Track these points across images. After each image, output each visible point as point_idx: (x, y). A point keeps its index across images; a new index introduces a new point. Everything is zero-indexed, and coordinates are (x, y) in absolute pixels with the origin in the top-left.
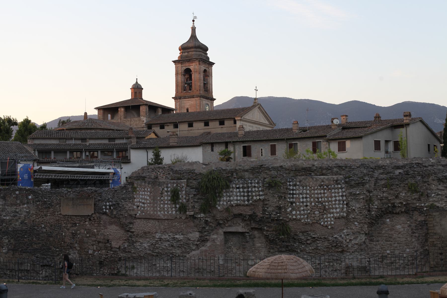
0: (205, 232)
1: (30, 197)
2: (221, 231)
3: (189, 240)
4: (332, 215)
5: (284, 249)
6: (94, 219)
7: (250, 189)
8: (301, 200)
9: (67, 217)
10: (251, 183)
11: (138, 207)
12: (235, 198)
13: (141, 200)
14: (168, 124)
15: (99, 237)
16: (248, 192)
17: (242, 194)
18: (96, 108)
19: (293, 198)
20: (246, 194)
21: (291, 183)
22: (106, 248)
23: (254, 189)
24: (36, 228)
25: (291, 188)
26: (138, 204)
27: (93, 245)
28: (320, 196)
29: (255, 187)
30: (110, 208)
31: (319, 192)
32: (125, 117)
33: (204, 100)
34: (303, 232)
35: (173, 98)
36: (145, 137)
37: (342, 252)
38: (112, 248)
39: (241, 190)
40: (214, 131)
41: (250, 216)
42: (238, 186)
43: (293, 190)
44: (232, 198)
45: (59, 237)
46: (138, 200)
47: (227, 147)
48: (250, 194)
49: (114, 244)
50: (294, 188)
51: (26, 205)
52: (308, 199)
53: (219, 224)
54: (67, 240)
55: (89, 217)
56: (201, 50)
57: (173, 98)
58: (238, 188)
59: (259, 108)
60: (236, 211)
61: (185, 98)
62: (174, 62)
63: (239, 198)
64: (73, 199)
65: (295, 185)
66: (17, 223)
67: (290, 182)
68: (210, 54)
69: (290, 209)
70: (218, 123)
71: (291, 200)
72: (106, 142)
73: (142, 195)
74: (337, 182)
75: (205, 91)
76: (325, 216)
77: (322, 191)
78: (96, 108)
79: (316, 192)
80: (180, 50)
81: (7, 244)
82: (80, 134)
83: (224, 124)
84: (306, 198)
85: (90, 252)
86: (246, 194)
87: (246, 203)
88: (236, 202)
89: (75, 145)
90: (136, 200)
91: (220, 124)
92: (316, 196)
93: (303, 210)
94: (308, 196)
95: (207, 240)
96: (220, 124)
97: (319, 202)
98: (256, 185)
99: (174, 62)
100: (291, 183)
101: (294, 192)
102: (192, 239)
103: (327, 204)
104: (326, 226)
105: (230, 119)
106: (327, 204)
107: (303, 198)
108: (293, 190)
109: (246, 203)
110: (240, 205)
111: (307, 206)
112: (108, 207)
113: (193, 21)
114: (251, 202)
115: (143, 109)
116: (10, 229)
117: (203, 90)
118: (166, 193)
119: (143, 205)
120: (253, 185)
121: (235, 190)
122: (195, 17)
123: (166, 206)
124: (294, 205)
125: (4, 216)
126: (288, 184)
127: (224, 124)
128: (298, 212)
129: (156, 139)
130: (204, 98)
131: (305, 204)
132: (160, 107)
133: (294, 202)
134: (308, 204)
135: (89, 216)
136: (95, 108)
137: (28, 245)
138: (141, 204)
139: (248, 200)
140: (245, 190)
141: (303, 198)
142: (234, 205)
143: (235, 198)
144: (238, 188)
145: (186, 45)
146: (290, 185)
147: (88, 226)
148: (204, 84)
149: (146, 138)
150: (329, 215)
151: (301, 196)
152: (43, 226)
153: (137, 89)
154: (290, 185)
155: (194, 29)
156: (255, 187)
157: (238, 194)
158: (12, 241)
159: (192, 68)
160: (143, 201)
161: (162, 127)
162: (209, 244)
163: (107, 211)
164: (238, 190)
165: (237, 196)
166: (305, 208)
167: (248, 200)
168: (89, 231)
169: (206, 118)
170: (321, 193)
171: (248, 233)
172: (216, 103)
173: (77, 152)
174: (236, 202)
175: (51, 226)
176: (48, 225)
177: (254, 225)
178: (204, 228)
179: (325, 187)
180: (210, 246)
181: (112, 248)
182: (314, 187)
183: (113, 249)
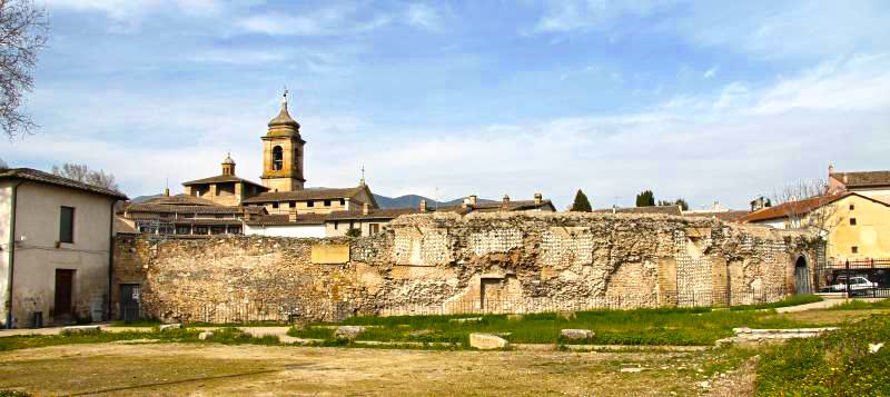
1: (275, 246)
18: (186, 185)
22: (362, 295)
32: (217, 194)
37: (586, 296)
40: (317, 212)
47: (352, 225)
54: (320, 289)
55: (344, 265)
60: (493, 258)
61: (274, 177)
70: (323, 203)
74: (585, 231)
78: (186, 185)
83: (329, 205)
85: (345, 300)
91: (326, 205)
96: (326, 205)
105: (336, 200)
115: (238, 187)
122: (287, 92)
127: (329, 205)
153: (230, 167)
159: (282, 145)
161: (276, 205)
162: (467, 289)
169: (327, 197)
172: (306, 186)
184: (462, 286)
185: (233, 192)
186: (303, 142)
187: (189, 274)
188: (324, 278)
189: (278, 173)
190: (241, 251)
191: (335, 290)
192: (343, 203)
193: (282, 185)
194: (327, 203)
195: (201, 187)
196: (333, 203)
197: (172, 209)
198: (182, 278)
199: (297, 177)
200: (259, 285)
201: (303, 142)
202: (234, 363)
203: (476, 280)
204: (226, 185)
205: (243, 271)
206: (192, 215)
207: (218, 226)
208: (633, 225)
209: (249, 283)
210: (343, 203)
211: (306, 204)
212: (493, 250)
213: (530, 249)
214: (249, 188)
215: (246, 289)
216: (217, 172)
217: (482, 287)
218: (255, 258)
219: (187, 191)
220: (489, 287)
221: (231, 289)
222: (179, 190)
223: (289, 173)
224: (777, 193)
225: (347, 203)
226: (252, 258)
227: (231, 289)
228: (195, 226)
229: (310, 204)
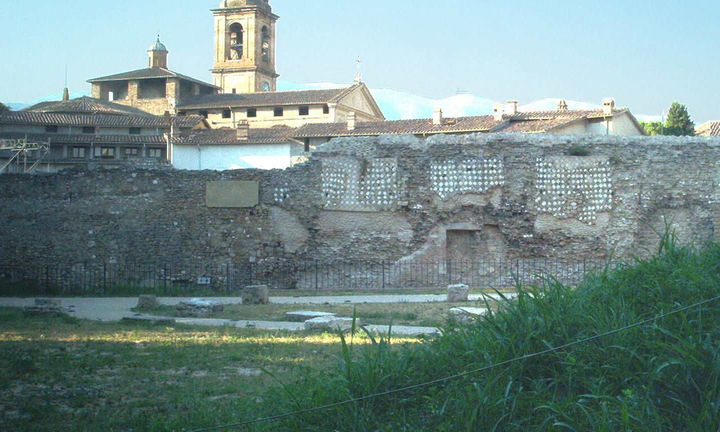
18: (94, 82)
22: (275, 253)
55: (251, 211)
83: (281, 114)
85: (252, 259)
91: (276, 115)
96: (276, 115)
105: (316, 106)
115: (171, 87)
127: (281, 114)
159: (243, 23)
162: (426, 246)
184: (418, 241)
185: (163, 94)
186: (274, 18)
188: (223, 228)
189: (235, 63)
192: (326, 110)
193: (242, 83)
194: (304, 111)
195: (118, 85)
196: (311, 112)
197: (62, 119)
199: (265, 67)
201: (274, 18)
202: (183, 324)
203: (439, 235)
204: (152, 84)
205: (110, 217)
208: (677, 153)
210: (326, 110)
211: (272, 113)
213: (517, 189)
214: (186, 86)
216: (143, 62)
217: (449, 243)
220: (460, 240)
222: (83, 90)
223: (252, 64)
224: (304, 282)
225: (332, 111)
229: (278, 112)
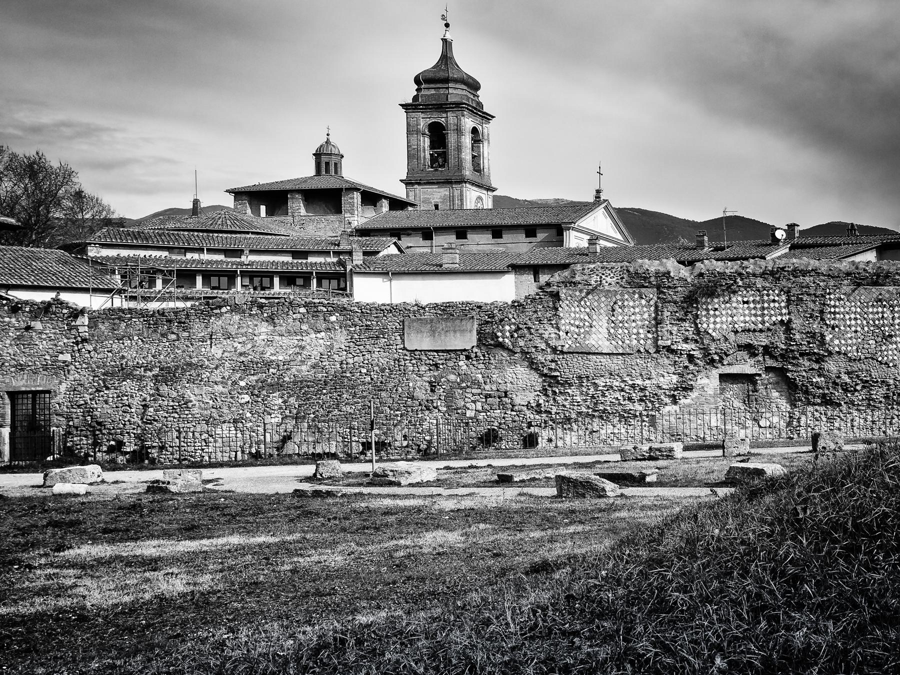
0: (688, 374)
1: (333, 318)
2: (715, 373)
3: (659, 387)
4: (895, 346)
5: (819, 401)
6: (476, 357)
7: (766, 305)
8: (848, 323)
9: (417, 353)
10: (768, 295)
11: (567, 333)
12: (742, 318)
13: (572, 322)
14: (410, 232)
15: (487, 387)
16: (763, 309)
17: (753, 312)
18: (238, 194)
19: (834, 319)
20: (759, 313)
21: (832, 297)
23: (772, 305)
24: (348, 375)
25: (832, 303)
26: (568, 327)
27: (474, 402)
28: (877, 316)
29: (774, 301)
30: (512, 336)
31: (875, 310)
33: (474, 188)
34: (848, 373)
35: (401, 181)
36: (378, 252)
38: (513, 406)
39: (752, 305)
41: (766, 348)
42: (745, 299)
43: (835, 306)
44: (735, 319)
45: (400, 389)
46: (568, 321)
48: (766, 312)
49: (520, 399)
50: (837, 304)
51: (323, 334)
52: (859, 322)
53: (712, 361)
54: (420, 394)
56: (465, 87)
57: (401, 181)
58: (747, 302)
59: (606, 208)
62: (405, 106)
63: (747, 319)
64: (432, 320)
65: (840, 299)
66: (304, 368)
67: (829, 294)
68: (484, 96)
69: (831, 336)
71: (832, 322)
72: (288, 259)
73: (575, 312)
75: (474, 170)
76: (883, 348)
77: (880, 309)
79: (871, 310)
80: (417, 81)
81: (280, 408)
82: (221, 241)
84: (856, 319)
85: (470, 414)
86: (759, 313)
87: (760, 326)
88: (742, 325)
89: (210, 262)
90: (563, 322)
92: (871, 316)
93: (851, 338)
94: (858, 316)
95: (690, 389)
97: (875, 325)
98: (777, 298)
99: (405, 106)
100: (832, 297)
101: (837, 310)
102: (664, 387)
103: (887, 329)
104: (886, 363)
106: (887, 329)
107: (850, 319)
108: (835, 306)
109: (760, 326)
110: (749, 330)
111: (856, 332)
112: (508, 334)
113: (447, 25)
114: (767, 324)
116: (287, 379)
117: (472, 168)
118: (620, 310)
119: (577, 330)
120: (772, 297)
121: (741, 306)
123: (620, 331)
124: (837, 329)
125: (272, 354)
126: (828, 297)
128: (843, 342)
129: (396, 255)
130: (473, 184)
131: (853, 329)
132: (386, 198)
133: (837, 326)
134: (859, 329)
135: (465, 350)
136: (227, 191)
137: (329, 407)
138: (572, 328)
139: (763, 323)
140: (759, 306)
141: (850, 319)
142: (740, 330)
143: (742, 318)
144: (747, 302)
145: (431, 75)
146: (830, 299)
147: (465, 367)
148: (474, 157)
149: (381, 254)
150: (891, 347)
151: (847, 317)
152: (364, 371)
154: (830, 299)
155: (447, 44)
156: (774, 301)
157: (747, 312)
158: (292, 400)
160: (577, 323)
162: (694, 394)
163: (507, 340)
164: (746, 306)
165: (745, 315)
166: (853, 335)
167: (763, 323)
168: (464, 377)
170: (877, 313)
171: (760, 375)
173: (219, 276)
174: (742, 325)
175: (383, 370)
176: (376, 368)
177: (770, 363)
178: (686, 367)
179: (884, 303)
180: (697, 397)
181: (513, 406)
182: (867, 303)
183: (516, 408)
187: (156, 371)
190: (264, 328)
191: (449, 397)
195: (273, 199)
198: (141, 379)
200: (300, 386)
205: (268, 364)
206: (238, 253)
207: (219, 274)
209: (278, 386)
212: (739, 326)
215: (276, 400)
216: (299, 169)
218: (294, 340)
219: (229, 201)
220: (554, 232)
221: (247, 398)
226: (286, 341)
227: (247, 398)
228: (244, 274)
